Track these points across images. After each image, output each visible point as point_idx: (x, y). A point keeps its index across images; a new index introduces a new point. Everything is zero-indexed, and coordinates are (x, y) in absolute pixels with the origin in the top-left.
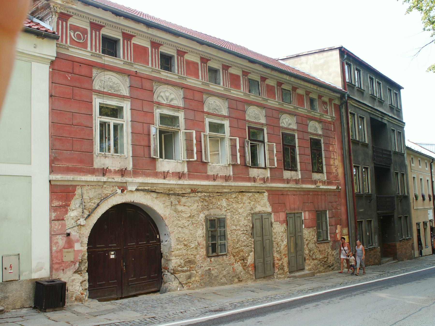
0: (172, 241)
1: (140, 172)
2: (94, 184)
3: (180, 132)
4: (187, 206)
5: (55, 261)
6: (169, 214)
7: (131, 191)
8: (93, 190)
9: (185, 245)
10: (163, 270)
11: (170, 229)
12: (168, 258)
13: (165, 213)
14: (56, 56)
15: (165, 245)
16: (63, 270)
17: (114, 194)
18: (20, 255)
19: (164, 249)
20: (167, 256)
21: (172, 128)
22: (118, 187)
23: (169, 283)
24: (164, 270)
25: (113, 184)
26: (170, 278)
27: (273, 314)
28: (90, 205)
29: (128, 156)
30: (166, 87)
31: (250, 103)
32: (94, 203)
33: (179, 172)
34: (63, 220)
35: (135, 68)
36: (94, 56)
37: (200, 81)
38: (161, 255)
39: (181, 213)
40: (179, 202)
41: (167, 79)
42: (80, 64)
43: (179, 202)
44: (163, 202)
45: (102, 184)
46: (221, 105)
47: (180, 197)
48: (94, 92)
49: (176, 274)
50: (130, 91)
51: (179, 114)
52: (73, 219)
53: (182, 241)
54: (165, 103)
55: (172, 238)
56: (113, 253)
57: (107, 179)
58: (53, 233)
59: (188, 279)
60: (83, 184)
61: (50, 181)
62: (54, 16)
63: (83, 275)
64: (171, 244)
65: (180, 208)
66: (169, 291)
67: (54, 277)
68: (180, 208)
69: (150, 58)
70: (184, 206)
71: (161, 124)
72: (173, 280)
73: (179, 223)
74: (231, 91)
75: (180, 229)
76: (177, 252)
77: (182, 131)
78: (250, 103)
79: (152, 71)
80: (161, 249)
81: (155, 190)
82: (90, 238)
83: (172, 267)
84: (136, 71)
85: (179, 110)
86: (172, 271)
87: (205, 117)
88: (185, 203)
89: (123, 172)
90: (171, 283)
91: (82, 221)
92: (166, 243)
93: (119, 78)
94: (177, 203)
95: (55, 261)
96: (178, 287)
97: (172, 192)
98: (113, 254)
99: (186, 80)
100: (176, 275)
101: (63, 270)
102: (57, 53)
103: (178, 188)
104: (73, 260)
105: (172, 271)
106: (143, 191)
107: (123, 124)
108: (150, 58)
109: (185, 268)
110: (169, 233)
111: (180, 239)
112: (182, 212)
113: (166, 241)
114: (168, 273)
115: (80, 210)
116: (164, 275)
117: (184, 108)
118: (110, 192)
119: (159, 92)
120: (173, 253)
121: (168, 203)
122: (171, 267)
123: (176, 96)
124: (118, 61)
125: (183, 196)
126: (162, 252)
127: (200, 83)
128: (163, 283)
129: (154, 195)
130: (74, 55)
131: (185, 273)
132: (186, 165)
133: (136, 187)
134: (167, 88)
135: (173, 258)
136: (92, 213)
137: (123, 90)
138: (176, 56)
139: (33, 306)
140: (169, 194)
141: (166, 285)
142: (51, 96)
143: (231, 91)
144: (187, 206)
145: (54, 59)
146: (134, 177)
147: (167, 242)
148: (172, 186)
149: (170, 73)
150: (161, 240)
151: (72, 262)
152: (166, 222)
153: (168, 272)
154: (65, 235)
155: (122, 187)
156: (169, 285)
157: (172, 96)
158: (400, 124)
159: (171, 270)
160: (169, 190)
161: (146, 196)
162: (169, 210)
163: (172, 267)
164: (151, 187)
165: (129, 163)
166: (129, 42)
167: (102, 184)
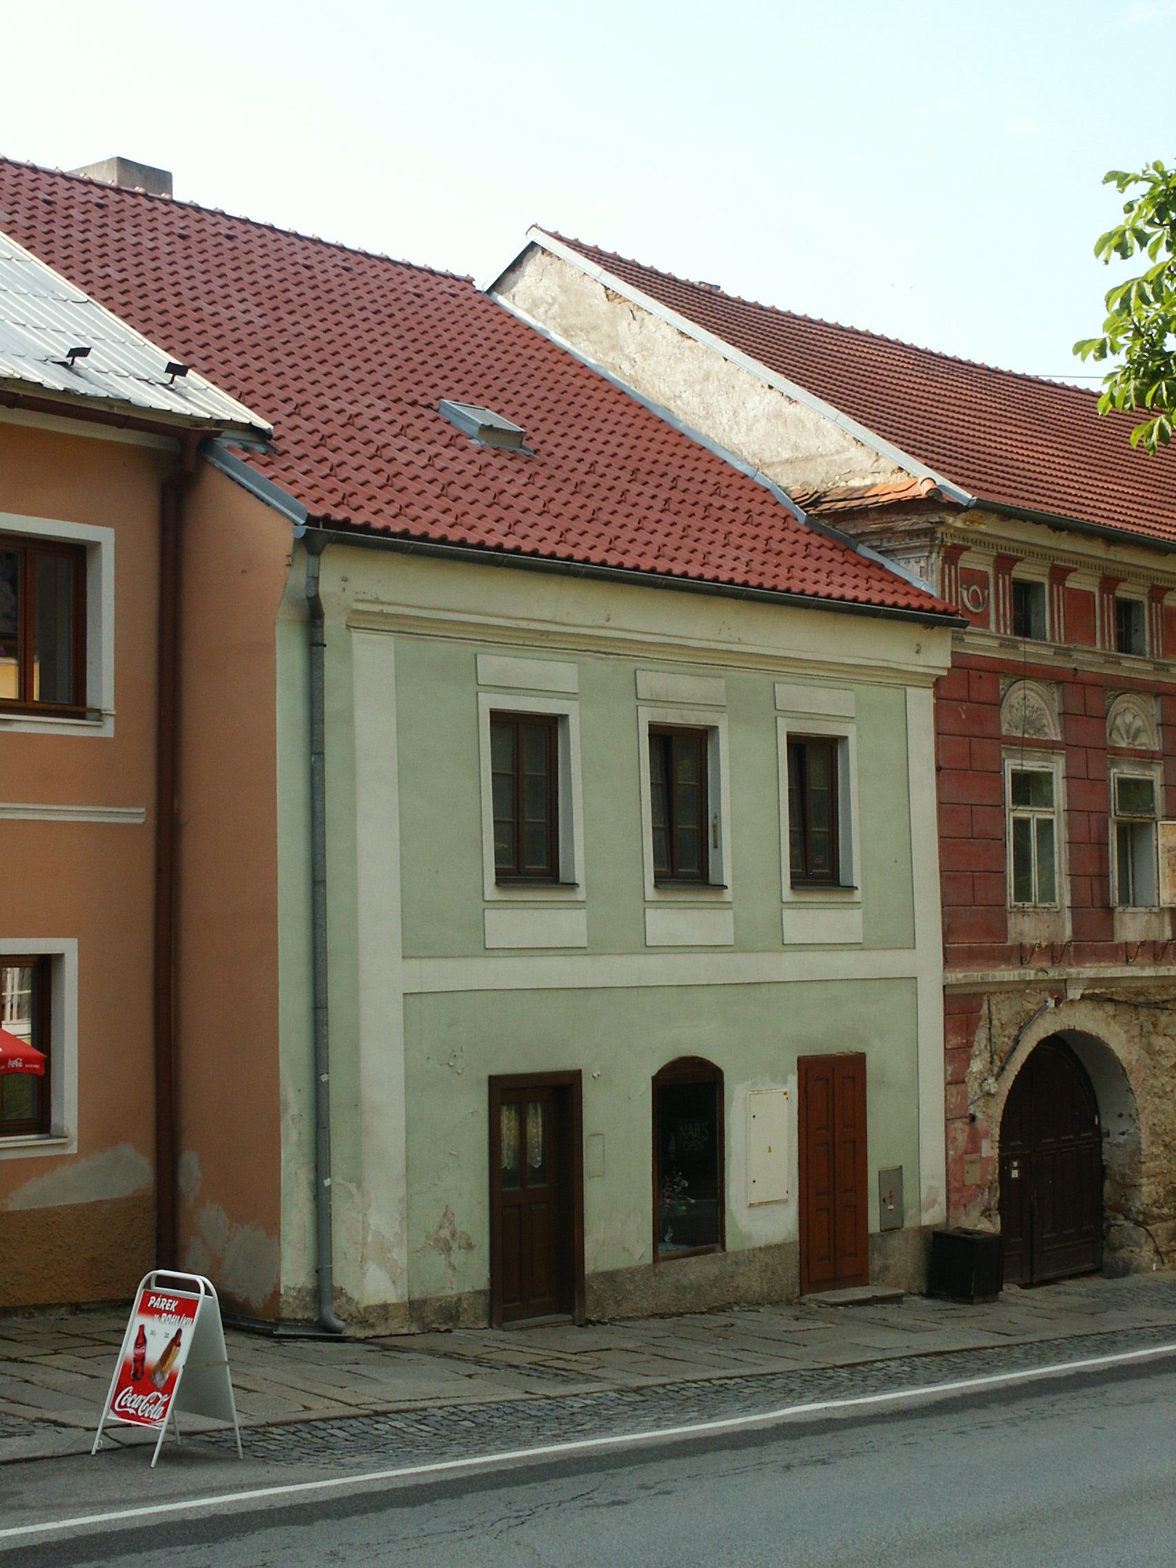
0: (1143, 1136)
1: (1088, 950)
2: (1008, 988)
3: (1154, 825)
4: (1169, 1036)
5: (955, 1184)
6: (1137, 1060)
7: (1072, 1001)
8: (1007, 1003)
9: (1166, 1146)
10: (1108, 1213)
11: (1138, 1100)
12: (1128, 1181)
13: (1129, 1058)
14: (949, 665)
15: (1118, 1145)
16: (965, 1206)
17: (1042, 1010)
18: (904, 1169)
19: (1112, 1155)
20: (1123, 1176)
21: (1141, 817)
22: (1049, 991)
23: (1130, 1248)
24: (1113, 1213)
25: (1042, 986)
26: (1135, 1237)
27: (940, 1419)
28: (1003, 1043)
29: (1062, 907)
30: (1126, 699)
31: (1022, 672)
32: (1009, 1038)
33: (1154, 942)
34: (963, 1082)
35: (1075, 661)
36: (1007, 646)
37: (993, 637)
38: (1101, 1172)
39: (1160, 1055)
40: (1155, 1025)
41: (1133, 676)
42: (979, 673)
43: (1155, 1025)
44: (1126, 1028)
45: (1023, 987)
46: (1045, 707)
47: (1158, 1012)
48: (1004, 743)
49: (1148, 1224)
50: (1064, 730)
51: (1152, 773)
52: (976, 1079)
53: (1160, 1135)
54: (1123, 745)
55: (1142, 1127)
56: (1015, 1164)
57: (1036, 974)
58: (949, 1116)
59: (1171, 1240)
60: (992, 989)
61: (944, 987)
62: (934, 555)
63: (993, 1219)
64: (1140, 1143)
65: (1159, 1042)
66: (1136, 1272)
67: (953, 1224)
68: (1159, 1042)
69: (1098, 623)
70: (1165, 1035)
71: (1121, 809)
72: (1143, 1240)
73: (1156, 1083)
74: (1171, 669)
75: (1157, 1100)
76: (1152, 1164)
77: (1159, 823)
78: (1022, 672)
79: (1105, 662)
80: (1101, 1154)
81: (1112, 993)
82: (1004, 1125)
83: (1142, 1204)
84: (1075, 669)
85: (1152, 763)
86: (1141, 1216)
87: (1003, 755)
88: (1166, 1027)
89: (1054, 953)
90: (1137, 1250)
91: (991, 1082)
92: (1122, 1139)
93: (1041, 692)
94: (1151, 1028)
95: (955, 1184)
96: (1152, 1261)
97: (1141, 999)
98: (1016, 1168)
99: (1168, 671)
100: (1148, 1228)
101: (965, 1206)
102: (954, 654)
103: (1154, 987)
104: (979, 1182)
105: (1141, 1218)
106: (1090, 999)
107: (1051, 821)
108: (1098, 623)
109: (1165, 1211)
110: (1134, 1112)
111: (1157, 1128)
112: (1161, 1052)
113: (1123, 1134)
114: (1125, 1223)
115: (987, 1055)
116: (1109, 1227)
117: (1164, 755)
118: (1035, 1007)
119: (1114, 714)
120: (1144, 1168)
121: (1135, 1031)
122: (1138, 1204)
123: (1147, 723)
124: (1141, 663)
125: (1162, 1009)
126: (1104, 1163)
127: (995, 643)
128: (1106, 1249)
129: (1110, 1009)
130: (970, 652)
131: (1166, 1225)
132: (1167, 919)
133: (1081, 991)
134: (1128, 702)
135: (1144, 1181)
136: (1007, 1062)
137: (1048, 726)
138: (1146, 602)
139: (925, 1291)
140: (1136, 1006)
141: (1123, 1254)
142: (939, 769)
143: (1171, 669)
144: (1169, 1036)
145: (945, 673)
146: (1077, 964)
147: (1125, 1137)
148: (1144, 983)
149: (1140, 660)
150: (1104, 1131)
151: (978, 1186)
152: (1132, 1082)
153: (1126, 1218)
154: (968, 1121)
155: (1058, 991)
156: (1130, 1255)
157: (1138, 723)
158: (1059, 601)
159: (1139, 1212)
160: (1137, 994)
161: (1096, 1014)
162: (1137, 1047)
163: (1142, 1204)
164: (1107, 988)
165: (1063, 927)
166: (953, 567)
167: (1023, 987)
